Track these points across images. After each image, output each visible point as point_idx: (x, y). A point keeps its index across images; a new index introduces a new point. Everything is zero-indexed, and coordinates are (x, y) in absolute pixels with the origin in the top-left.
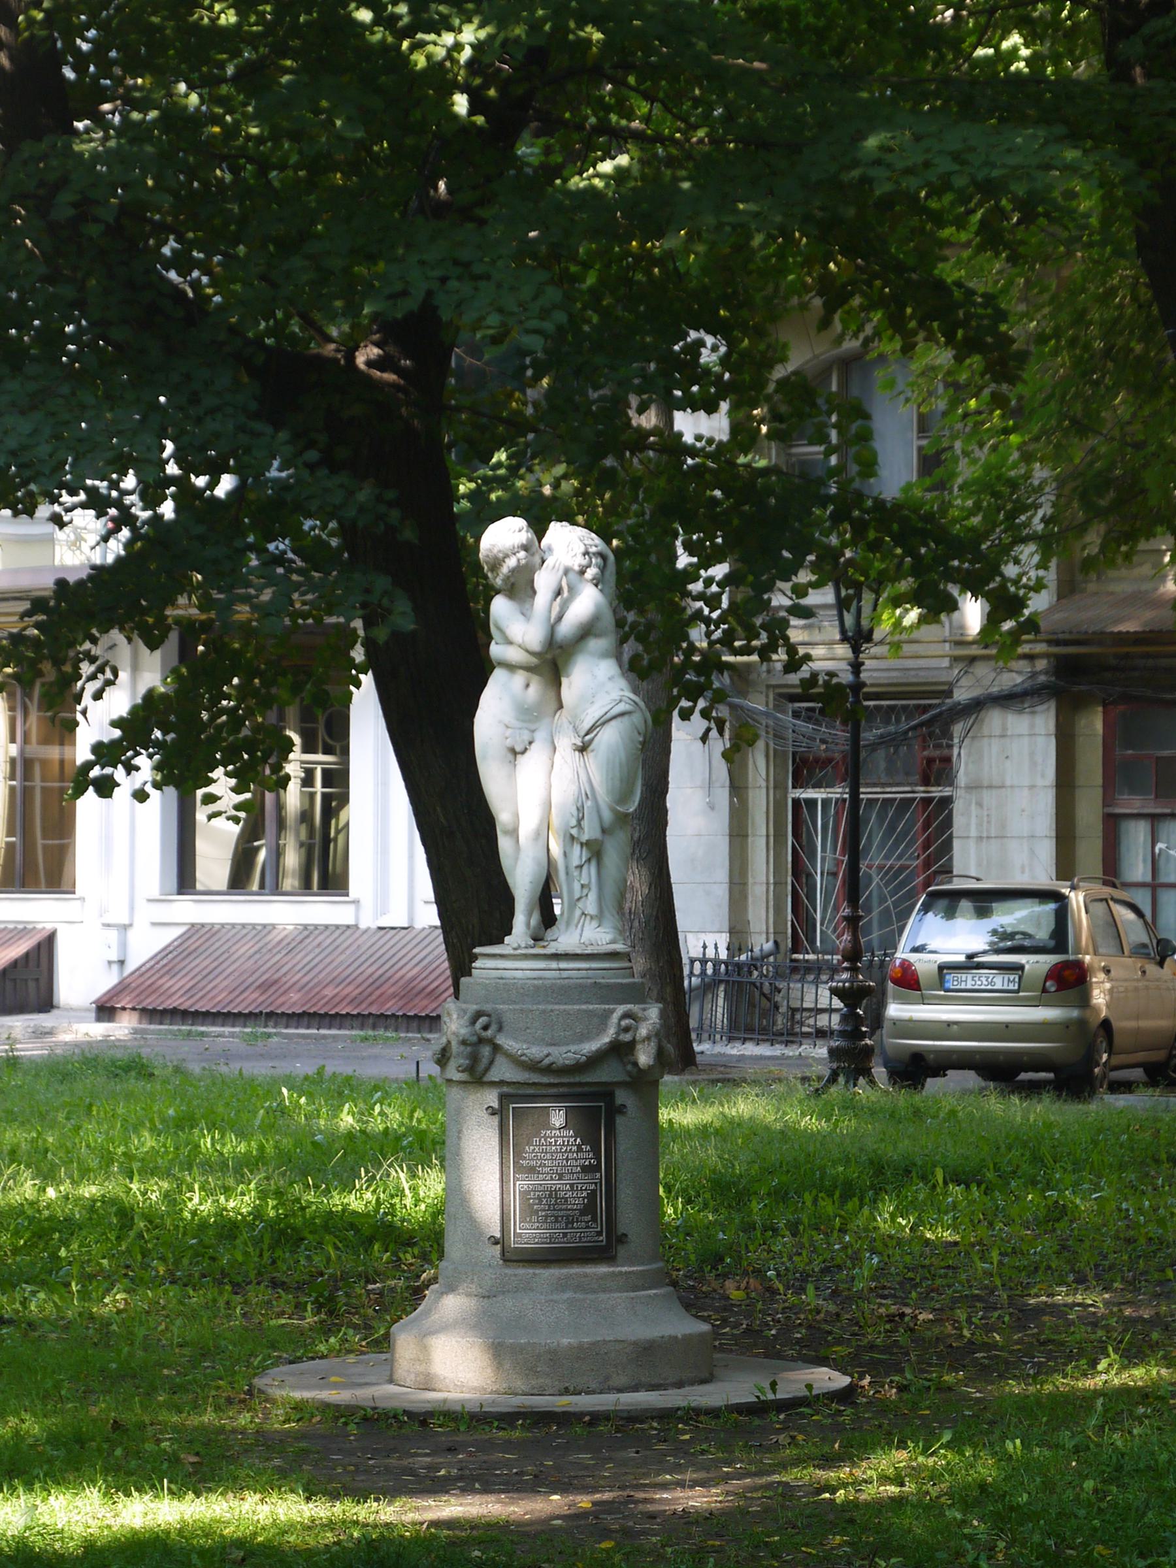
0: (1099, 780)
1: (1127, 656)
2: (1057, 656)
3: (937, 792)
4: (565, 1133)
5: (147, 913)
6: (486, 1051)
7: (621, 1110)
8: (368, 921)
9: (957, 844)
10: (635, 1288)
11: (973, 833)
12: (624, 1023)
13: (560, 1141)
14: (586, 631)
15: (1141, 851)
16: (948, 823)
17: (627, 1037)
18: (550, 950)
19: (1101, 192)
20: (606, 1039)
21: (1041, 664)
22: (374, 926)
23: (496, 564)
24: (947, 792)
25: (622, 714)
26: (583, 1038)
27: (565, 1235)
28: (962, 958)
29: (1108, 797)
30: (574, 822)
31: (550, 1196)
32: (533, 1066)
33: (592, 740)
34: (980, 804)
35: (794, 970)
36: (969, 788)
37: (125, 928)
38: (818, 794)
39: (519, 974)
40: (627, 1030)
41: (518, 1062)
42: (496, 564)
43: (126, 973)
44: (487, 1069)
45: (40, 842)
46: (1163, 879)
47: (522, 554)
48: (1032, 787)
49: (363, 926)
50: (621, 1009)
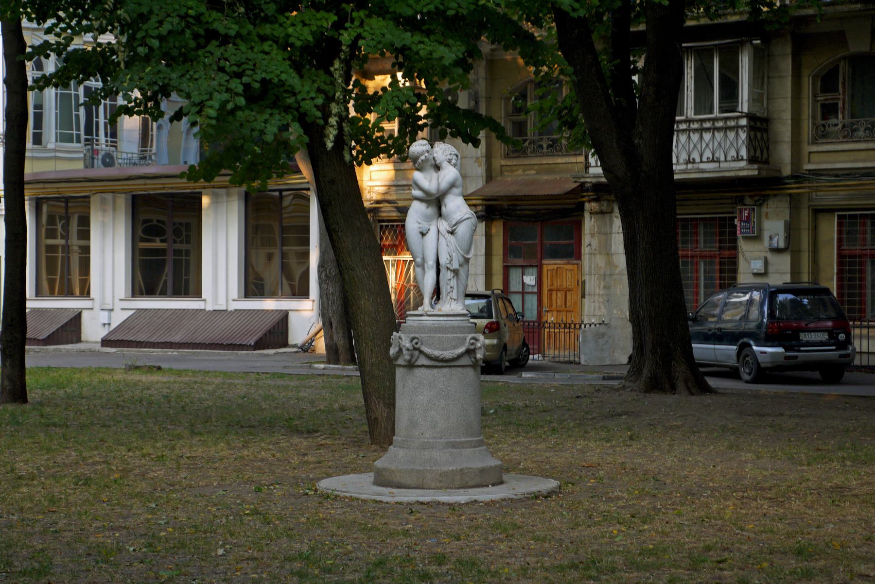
2: (486, 205)
5: (119, 305)
8: (210, 307)
10: (475, 447)
12: (473, 341)
17: (472, 347)
21: (480, 208)
22: (211, 309)
26: (455, 347)
29: (505, 259)
37: (112, 310)
40: (472, 344)
43: (111, 329)
45: (58, 277)
47: (427, 154)
49: (207, 309)
50: (470, 336)
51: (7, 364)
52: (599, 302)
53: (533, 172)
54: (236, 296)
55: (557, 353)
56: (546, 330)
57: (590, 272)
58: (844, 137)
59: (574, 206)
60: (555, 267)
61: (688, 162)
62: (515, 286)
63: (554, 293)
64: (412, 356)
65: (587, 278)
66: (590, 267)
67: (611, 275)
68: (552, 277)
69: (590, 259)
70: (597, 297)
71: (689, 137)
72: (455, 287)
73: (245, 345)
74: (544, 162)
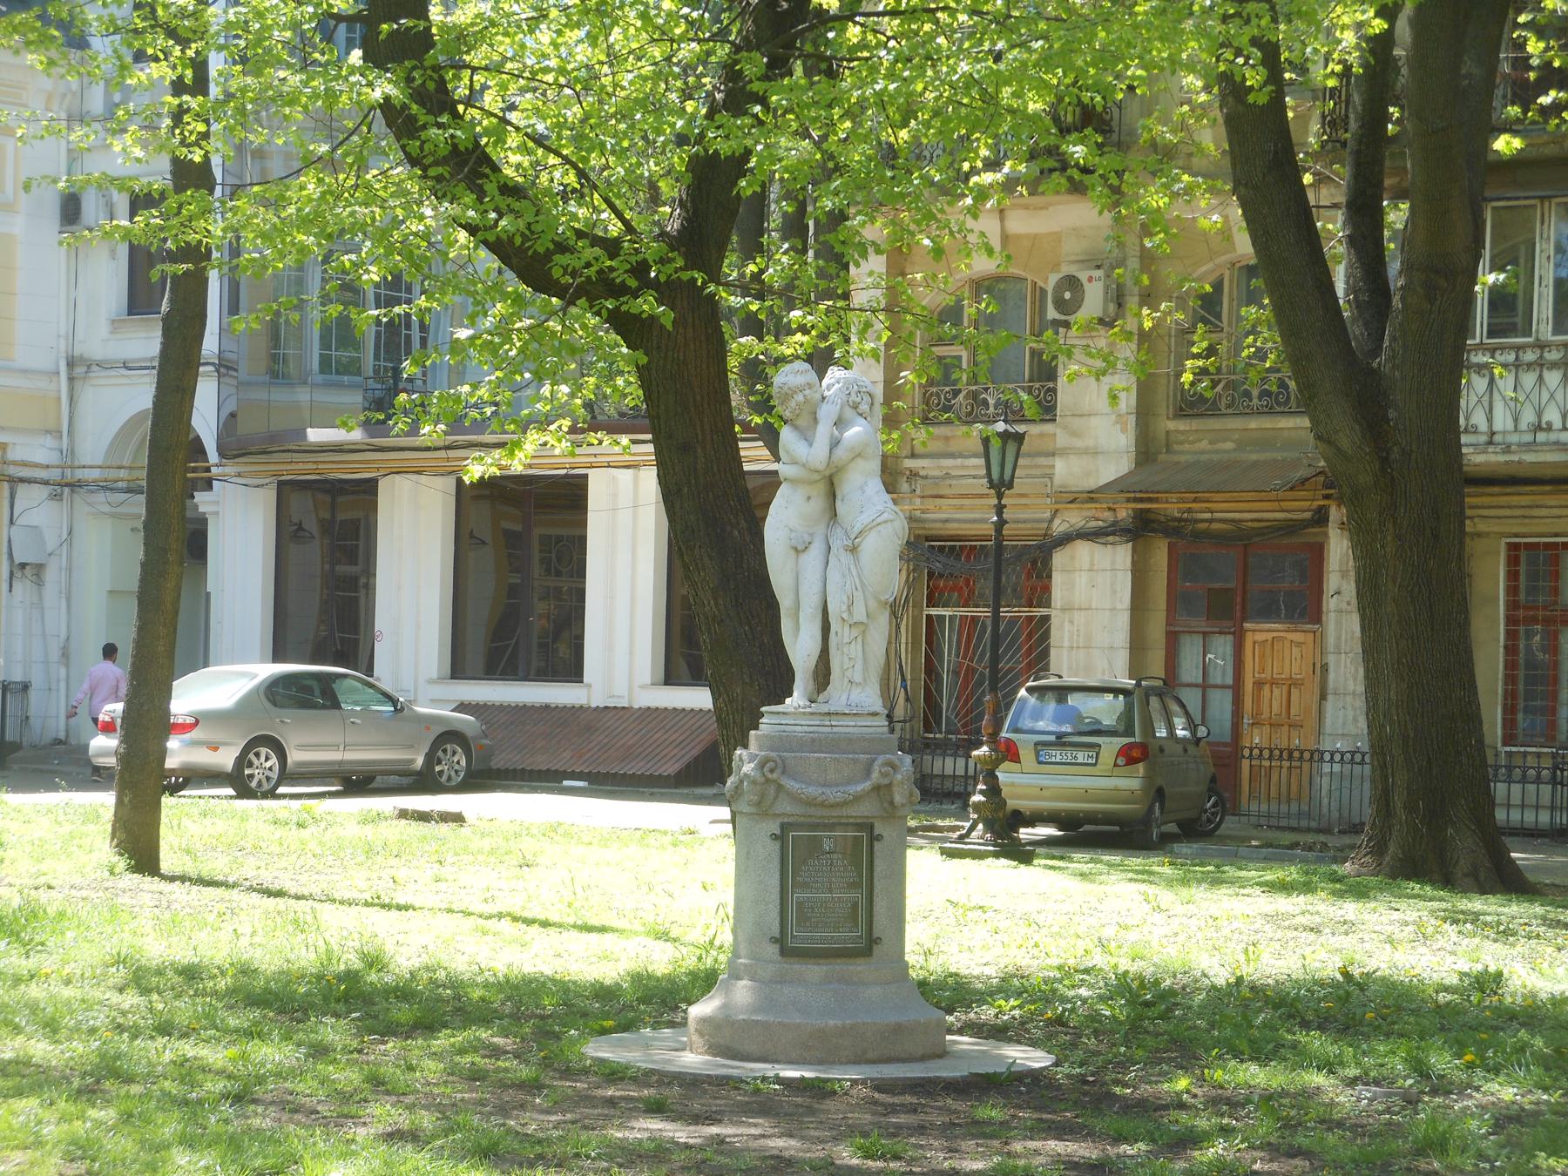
0: (1163, 606)
1: (1189, 510)
3: (1039, 612)
6: (772, 790)
7: (879, 838)
8: (597, 700)
9: (1053, 652)
11: (1066, 644)
16: (1046, 635)
17: (886, 781)
18: (825, 709)
20: (867, 785)
23: (787, 397)
24: (1043, 611)
28: (1052, 738)
29: (1170, 620)
30: (844, 608)
32: (810, 803)
34: (1071, 622)
35: (927, 746)
36: (1063, 610)
38: (946, 612)
41: (796, 798)
42: (787, 397)
46: (1211, 681)
48: (1113, 609)
51: (126, 800)
52: (1354, 709)
53: (1229, 445)
54: (647, 678)
55: (1284, 808)
56: (1245, 764)
57: (1338, 647)
59: (1308, 515)
60: (1270, 636)
61: (1538, 428)
62: (1190, 670)
63: (1267, 688)
65: (1331, 659)
66: (1338, 638)
68: (1262, 657)
70: (1349, 699)
71: (1541, 377)
73: (556, 771)
74: (1268, 425)
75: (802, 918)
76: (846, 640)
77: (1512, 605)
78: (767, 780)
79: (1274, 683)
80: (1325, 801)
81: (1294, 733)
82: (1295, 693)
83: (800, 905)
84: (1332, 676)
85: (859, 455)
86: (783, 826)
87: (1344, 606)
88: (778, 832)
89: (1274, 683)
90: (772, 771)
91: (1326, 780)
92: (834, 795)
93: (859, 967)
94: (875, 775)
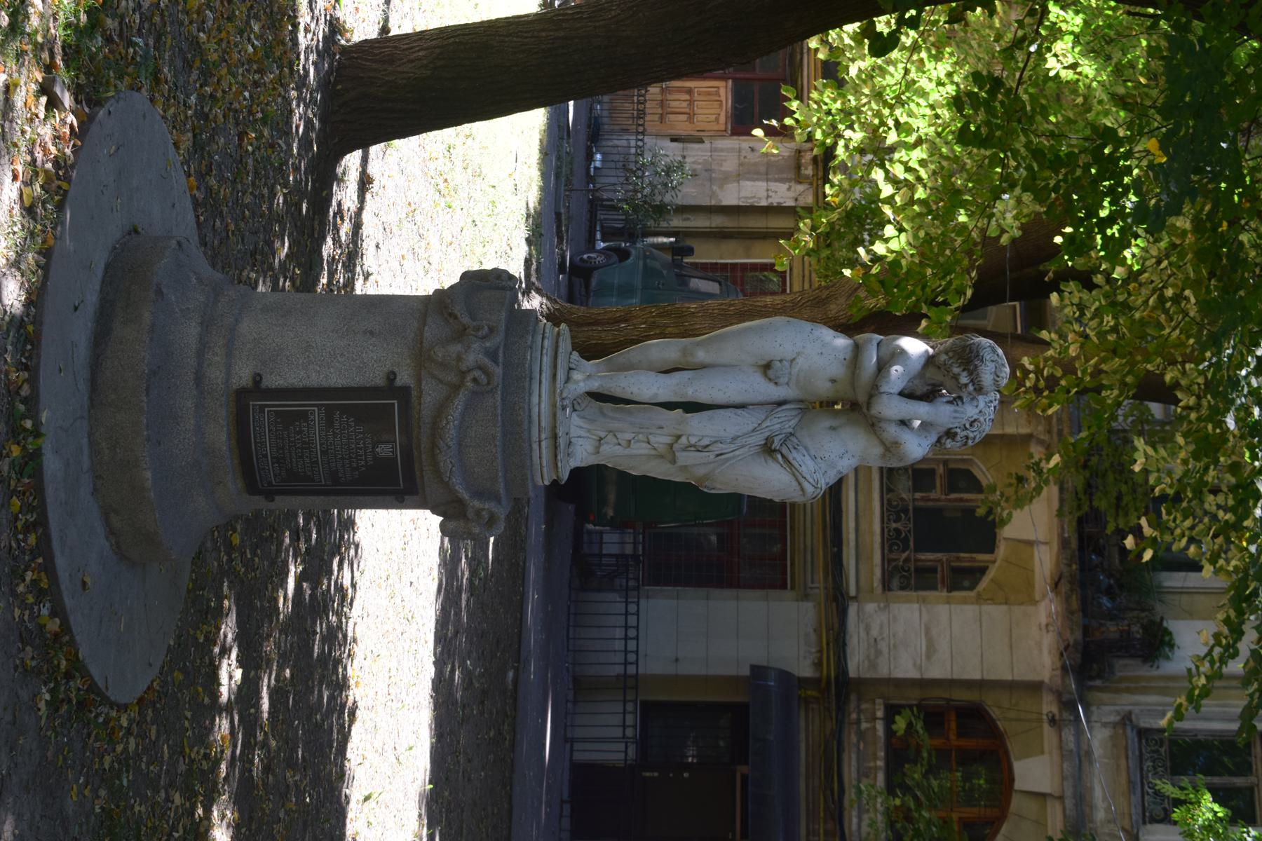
4: (370, 458)
6: (451, 378)
13: (361, 452)
14: (890, 448)
15: (707, 224)
17: (470, 514)
19: (985, 73)
20: (466, 496)
25: (802, 489)
27: (266, 456)
30: (693, 440)
31: (304, 443)
33: (776, 460)
39: (535, 399)
41: (441, 409)
44: (434, 377)
58: (889, 500)
63: (687, 97)
64: (443, 365)
65: (707, 145)
66: (722, 150)
67: (711, 180)
68: (709, 94)
69: (732, 150)
72: (627, 451)
75: (287, 419)
76: (652, 438)
77: (744, 267)
78: (463, 374)
79: (691, 102)
80: (610, 143)
81: (656, 117)
82: (684, 117)
83: (304, 416)
84: (696, 146)
85: (887, 449)
86: (405, 390)
87: (744, 154)
88: (399, 382)
89: (691, 102)
90: (475, 380)
91: (624, 143)
92: (447, 461)
93: (232, 484)
94: (477, 504)
